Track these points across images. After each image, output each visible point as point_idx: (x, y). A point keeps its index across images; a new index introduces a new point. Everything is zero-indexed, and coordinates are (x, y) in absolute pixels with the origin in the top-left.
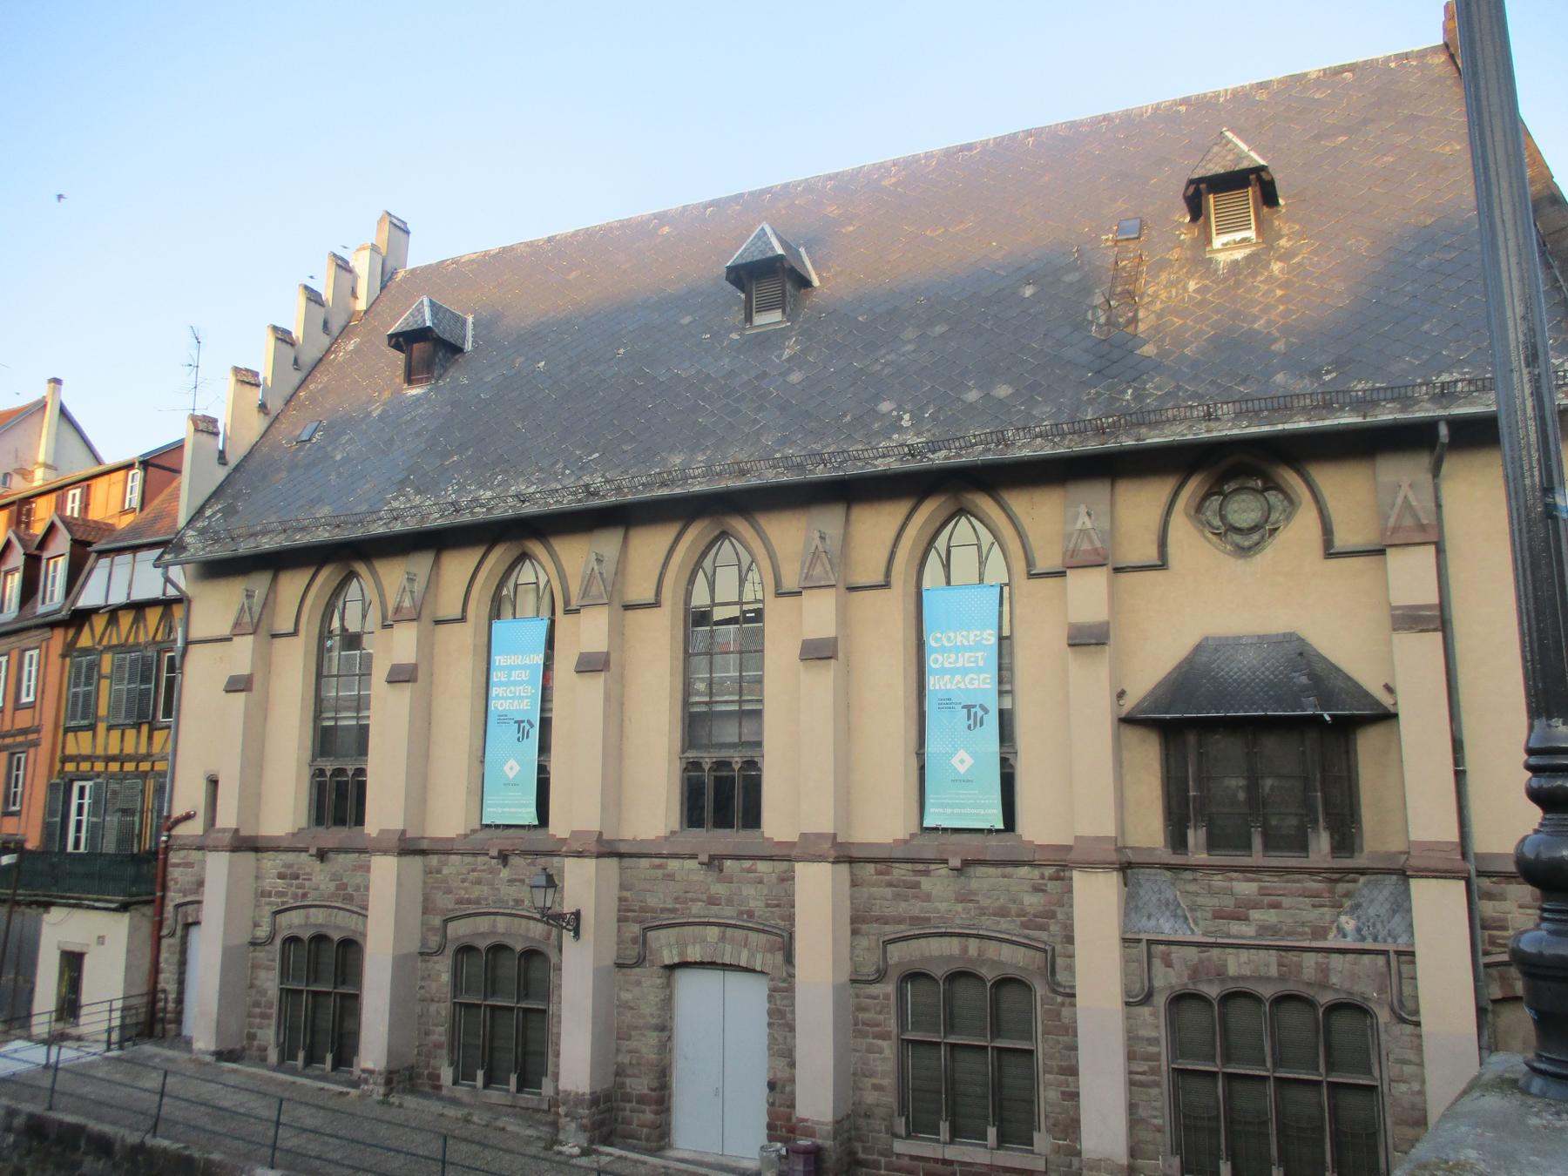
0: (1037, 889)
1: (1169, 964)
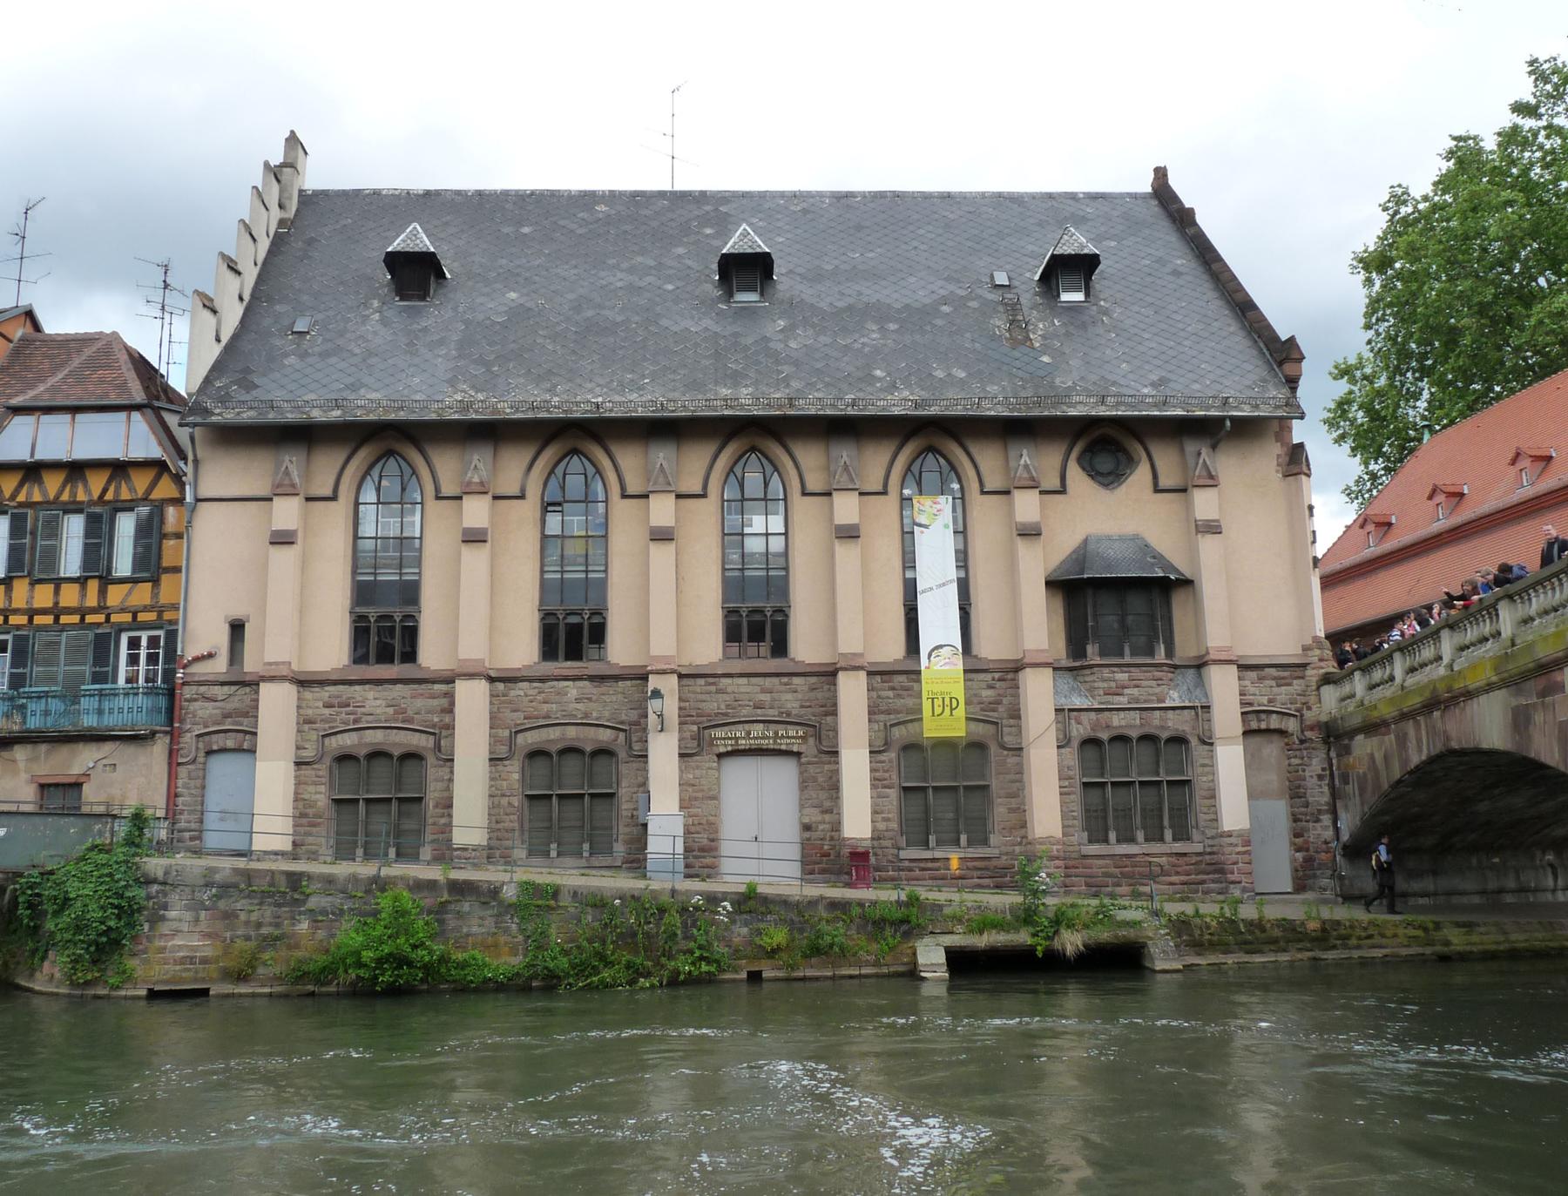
0: (990, 687)
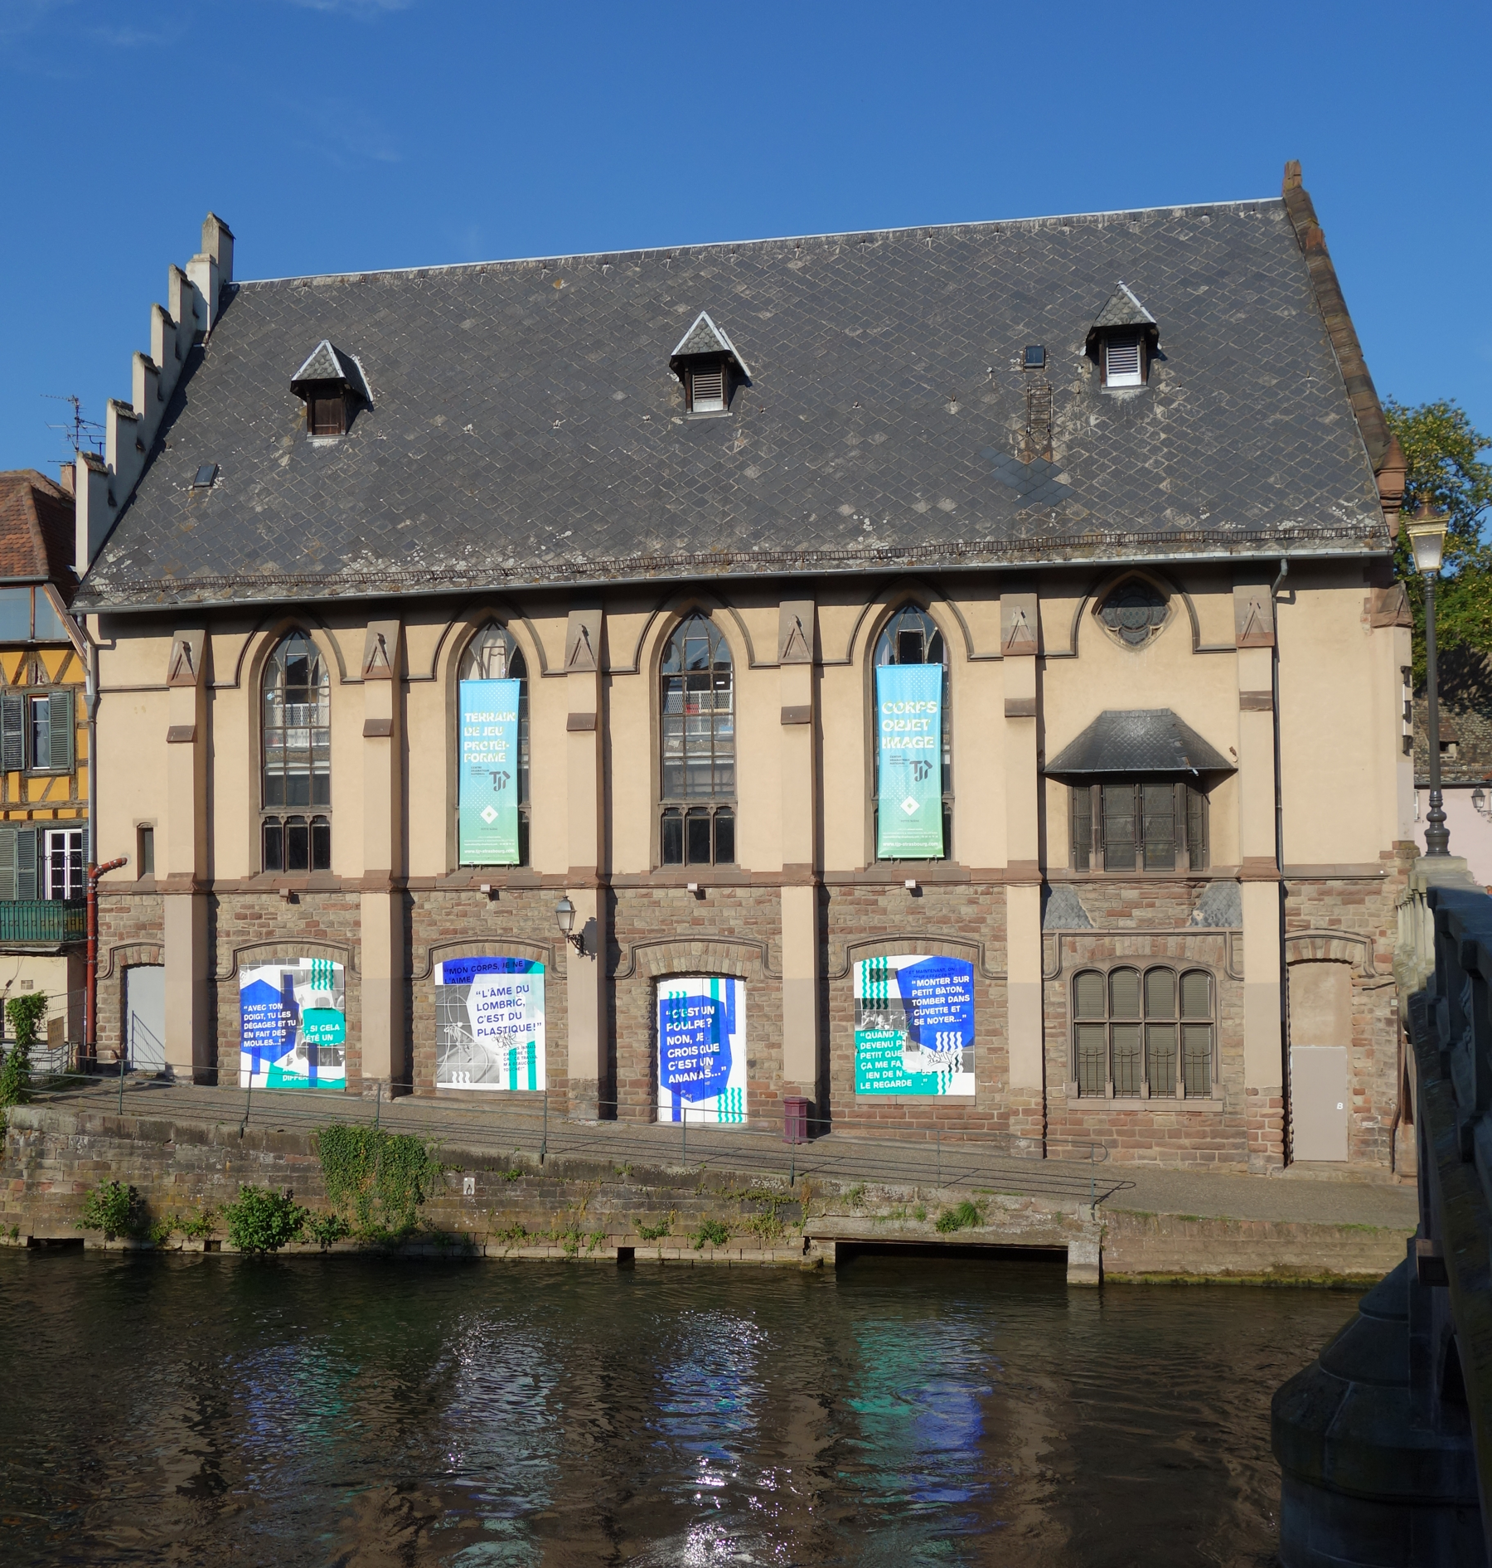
1: (1074, 950)
